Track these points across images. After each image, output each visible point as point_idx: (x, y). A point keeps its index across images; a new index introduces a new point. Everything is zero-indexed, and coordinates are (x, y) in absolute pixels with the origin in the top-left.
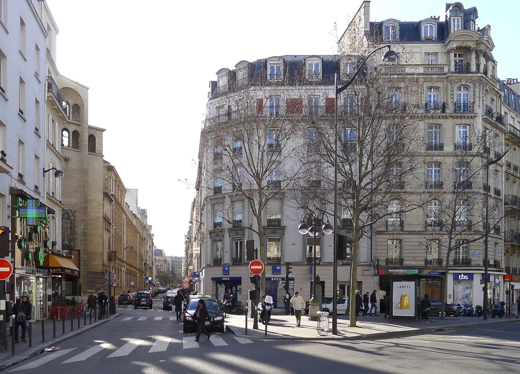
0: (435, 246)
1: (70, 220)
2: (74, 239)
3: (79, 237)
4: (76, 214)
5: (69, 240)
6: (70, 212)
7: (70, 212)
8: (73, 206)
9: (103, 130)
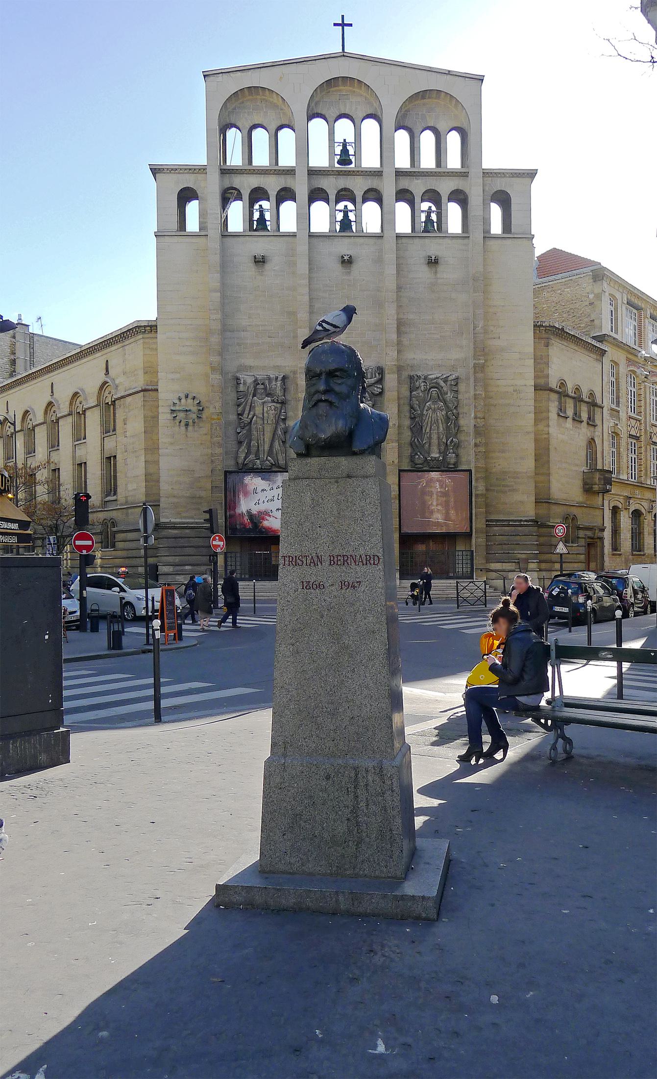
0: (467, 396)
1: (445, 402)
2: (457, 446)
3: (468, 439)
4: (462, 387)
5: (442, 448)
6: (442, 384)
7: (442, 384)
8: (454, 368)
9: (531, 174)
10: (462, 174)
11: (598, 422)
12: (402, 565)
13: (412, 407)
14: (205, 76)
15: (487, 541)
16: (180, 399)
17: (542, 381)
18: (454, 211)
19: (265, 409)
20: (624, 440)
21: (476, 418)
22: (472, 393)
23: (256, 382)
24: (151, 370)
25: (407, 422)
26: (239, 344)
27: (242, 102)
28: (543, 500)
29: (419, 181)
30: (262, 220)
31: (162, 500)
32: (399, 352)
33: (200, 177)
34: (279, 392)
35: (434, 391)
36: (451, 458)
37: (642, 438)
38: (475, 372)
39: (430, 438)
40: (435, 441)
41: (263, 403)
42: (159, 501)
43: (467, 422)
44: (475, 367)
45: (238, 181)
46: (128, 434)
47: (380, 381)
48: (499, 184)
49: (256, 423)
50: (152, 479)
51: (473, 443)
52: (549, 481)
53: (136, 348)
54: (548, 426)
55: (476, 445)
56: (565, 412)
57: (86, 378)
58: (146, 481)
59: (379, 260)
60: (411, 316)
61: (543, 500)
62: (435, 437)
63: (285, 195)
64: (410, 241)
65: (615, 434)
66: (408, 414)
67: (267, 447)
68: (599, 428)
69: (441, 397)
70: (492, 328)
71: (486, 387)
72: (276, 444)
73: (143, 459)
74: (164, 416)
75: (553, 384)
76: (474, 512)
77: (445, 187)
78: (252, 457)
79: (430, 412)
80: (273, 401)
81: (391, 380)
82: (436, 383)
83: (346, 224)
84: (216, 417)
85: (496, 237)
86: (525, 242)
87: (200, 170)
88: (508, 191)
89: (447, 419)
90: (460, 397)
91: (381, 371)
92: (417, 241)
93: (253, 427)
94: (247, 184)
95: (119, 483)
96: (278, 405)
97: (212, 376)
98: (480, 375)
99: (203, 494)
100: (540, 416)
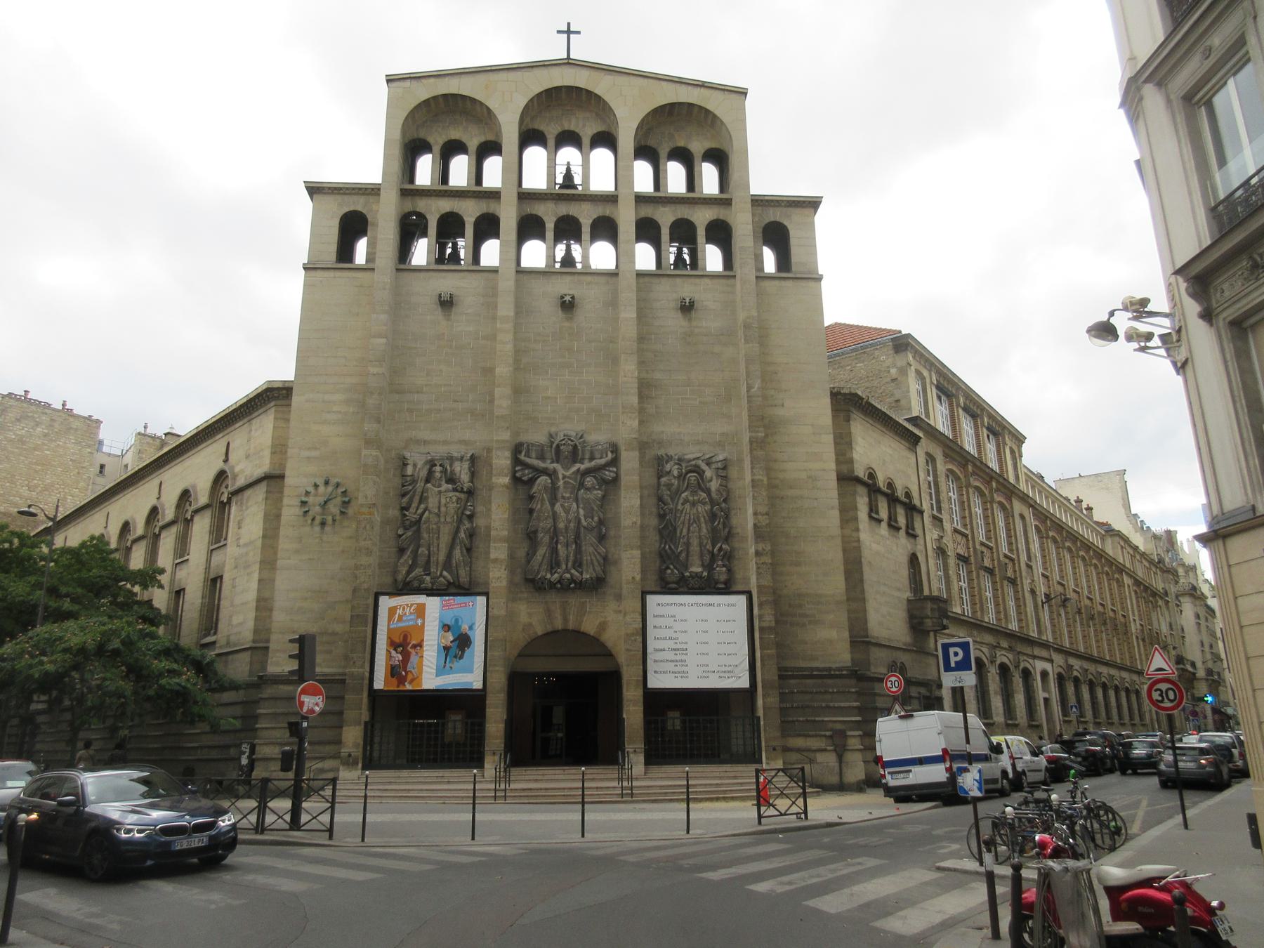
1: (708, 492)
4: (733, 472)
5: (707, 558)
6: (704, 466)
9: (813, 204)
10: (723, 202)
11: (919, 531)
12: (648, 740)
13: (660, 499)
14: (388, 81)
15: (781, 701)
16: (316, 486)
17: (844, 468)
18: (713, 258)
19: (443, 501)
20: (952, 561)
21: (755, 514)
22: (748, 478)
23: (432, 464)
24: (280, 448)
25: (654, 522)
26: (410, 411)
27: (438, 116)
28: (861, 640)
29: (667, 209)
30: (455, 257)
31: (274, 637)
32: (641, 422)
33: (372, 199)
34: (465, 477)
35: (692, 477)
36: (720, 572)
37: (972, 559)
38: (751, 450)
39: (688, 544)
40: (695, 548)
41: (440, 492)
42: (268, 641)
43: (746, 518)
44: (751, 442)
45: (422, 205)
46: (242, 542)
47: (615, 462)
48: (773, 215)
49: (428, 520)
50: (264, 606)
51: (752, 550)
52: (865, 611)
53: (263, 427)
54: (858, 530)
55: (757, 553)
56: (877, 513)
57: (196, 473)
58: (257, 609)
59: (613, 302)
60: (658, 375)
61: (861, 640)
62: (695, 542)
63: (488, 227)
64: (655, 280)
65: (941, 551)
66: (654, 510)
67: (442, 557)
68: (920, 540)
69: (701, 485)
70: (772, 392)
71: (768, 470)
72: (457, 553)
73: (256, 576)
74: (290, 511)
75: (860, 472)
76: (758, 654)
77: (700, 218)
78: (418, 571)
79: (687, 506)
80: (455, 490)
81: (630, 462)
82: (696, 466)
83: (568, 261)
84: (365, 510)
85: (770, 277)
86: (811, 284)
87: (371, 191)
88: (782, 225)
89: (713, 516)
90: (731, 485)
91: (614, 448)
92: (664, 280)
93: (424, 527)
94: (434, 210)
95: (221, 615)
96: (463, 496)
97: (364, 452)
98: (760, 453)
99: (339, 628)
100: (847, 516)
